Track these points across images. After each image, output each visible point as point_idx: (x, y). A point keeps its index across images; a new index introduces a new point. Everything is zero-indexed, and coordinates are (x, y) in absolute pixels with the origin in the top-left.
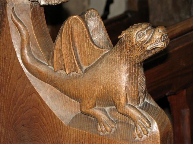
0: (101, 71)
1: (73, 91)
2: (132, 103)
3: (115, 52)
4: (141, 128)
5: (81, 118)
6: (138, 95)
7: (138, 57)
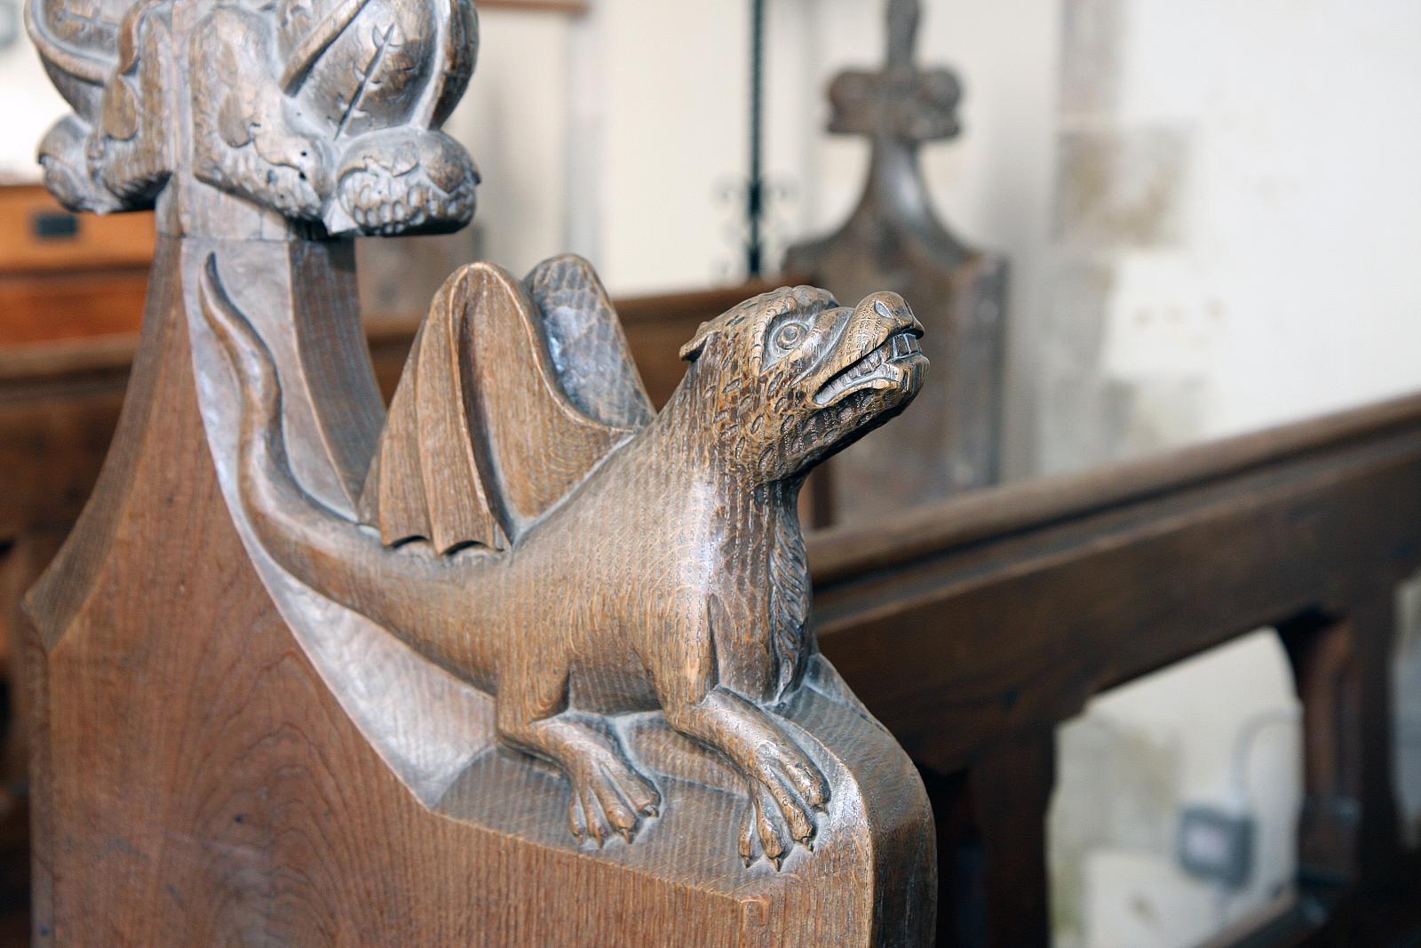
0: (593, 526)
1: (461, 637)
2: (738, 682)
3: (662, 430)
4: (781, 808)
5: (499, 771)
6: (769, 645)
7: (770, 448)
